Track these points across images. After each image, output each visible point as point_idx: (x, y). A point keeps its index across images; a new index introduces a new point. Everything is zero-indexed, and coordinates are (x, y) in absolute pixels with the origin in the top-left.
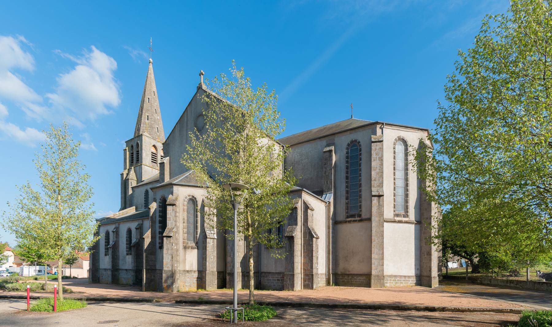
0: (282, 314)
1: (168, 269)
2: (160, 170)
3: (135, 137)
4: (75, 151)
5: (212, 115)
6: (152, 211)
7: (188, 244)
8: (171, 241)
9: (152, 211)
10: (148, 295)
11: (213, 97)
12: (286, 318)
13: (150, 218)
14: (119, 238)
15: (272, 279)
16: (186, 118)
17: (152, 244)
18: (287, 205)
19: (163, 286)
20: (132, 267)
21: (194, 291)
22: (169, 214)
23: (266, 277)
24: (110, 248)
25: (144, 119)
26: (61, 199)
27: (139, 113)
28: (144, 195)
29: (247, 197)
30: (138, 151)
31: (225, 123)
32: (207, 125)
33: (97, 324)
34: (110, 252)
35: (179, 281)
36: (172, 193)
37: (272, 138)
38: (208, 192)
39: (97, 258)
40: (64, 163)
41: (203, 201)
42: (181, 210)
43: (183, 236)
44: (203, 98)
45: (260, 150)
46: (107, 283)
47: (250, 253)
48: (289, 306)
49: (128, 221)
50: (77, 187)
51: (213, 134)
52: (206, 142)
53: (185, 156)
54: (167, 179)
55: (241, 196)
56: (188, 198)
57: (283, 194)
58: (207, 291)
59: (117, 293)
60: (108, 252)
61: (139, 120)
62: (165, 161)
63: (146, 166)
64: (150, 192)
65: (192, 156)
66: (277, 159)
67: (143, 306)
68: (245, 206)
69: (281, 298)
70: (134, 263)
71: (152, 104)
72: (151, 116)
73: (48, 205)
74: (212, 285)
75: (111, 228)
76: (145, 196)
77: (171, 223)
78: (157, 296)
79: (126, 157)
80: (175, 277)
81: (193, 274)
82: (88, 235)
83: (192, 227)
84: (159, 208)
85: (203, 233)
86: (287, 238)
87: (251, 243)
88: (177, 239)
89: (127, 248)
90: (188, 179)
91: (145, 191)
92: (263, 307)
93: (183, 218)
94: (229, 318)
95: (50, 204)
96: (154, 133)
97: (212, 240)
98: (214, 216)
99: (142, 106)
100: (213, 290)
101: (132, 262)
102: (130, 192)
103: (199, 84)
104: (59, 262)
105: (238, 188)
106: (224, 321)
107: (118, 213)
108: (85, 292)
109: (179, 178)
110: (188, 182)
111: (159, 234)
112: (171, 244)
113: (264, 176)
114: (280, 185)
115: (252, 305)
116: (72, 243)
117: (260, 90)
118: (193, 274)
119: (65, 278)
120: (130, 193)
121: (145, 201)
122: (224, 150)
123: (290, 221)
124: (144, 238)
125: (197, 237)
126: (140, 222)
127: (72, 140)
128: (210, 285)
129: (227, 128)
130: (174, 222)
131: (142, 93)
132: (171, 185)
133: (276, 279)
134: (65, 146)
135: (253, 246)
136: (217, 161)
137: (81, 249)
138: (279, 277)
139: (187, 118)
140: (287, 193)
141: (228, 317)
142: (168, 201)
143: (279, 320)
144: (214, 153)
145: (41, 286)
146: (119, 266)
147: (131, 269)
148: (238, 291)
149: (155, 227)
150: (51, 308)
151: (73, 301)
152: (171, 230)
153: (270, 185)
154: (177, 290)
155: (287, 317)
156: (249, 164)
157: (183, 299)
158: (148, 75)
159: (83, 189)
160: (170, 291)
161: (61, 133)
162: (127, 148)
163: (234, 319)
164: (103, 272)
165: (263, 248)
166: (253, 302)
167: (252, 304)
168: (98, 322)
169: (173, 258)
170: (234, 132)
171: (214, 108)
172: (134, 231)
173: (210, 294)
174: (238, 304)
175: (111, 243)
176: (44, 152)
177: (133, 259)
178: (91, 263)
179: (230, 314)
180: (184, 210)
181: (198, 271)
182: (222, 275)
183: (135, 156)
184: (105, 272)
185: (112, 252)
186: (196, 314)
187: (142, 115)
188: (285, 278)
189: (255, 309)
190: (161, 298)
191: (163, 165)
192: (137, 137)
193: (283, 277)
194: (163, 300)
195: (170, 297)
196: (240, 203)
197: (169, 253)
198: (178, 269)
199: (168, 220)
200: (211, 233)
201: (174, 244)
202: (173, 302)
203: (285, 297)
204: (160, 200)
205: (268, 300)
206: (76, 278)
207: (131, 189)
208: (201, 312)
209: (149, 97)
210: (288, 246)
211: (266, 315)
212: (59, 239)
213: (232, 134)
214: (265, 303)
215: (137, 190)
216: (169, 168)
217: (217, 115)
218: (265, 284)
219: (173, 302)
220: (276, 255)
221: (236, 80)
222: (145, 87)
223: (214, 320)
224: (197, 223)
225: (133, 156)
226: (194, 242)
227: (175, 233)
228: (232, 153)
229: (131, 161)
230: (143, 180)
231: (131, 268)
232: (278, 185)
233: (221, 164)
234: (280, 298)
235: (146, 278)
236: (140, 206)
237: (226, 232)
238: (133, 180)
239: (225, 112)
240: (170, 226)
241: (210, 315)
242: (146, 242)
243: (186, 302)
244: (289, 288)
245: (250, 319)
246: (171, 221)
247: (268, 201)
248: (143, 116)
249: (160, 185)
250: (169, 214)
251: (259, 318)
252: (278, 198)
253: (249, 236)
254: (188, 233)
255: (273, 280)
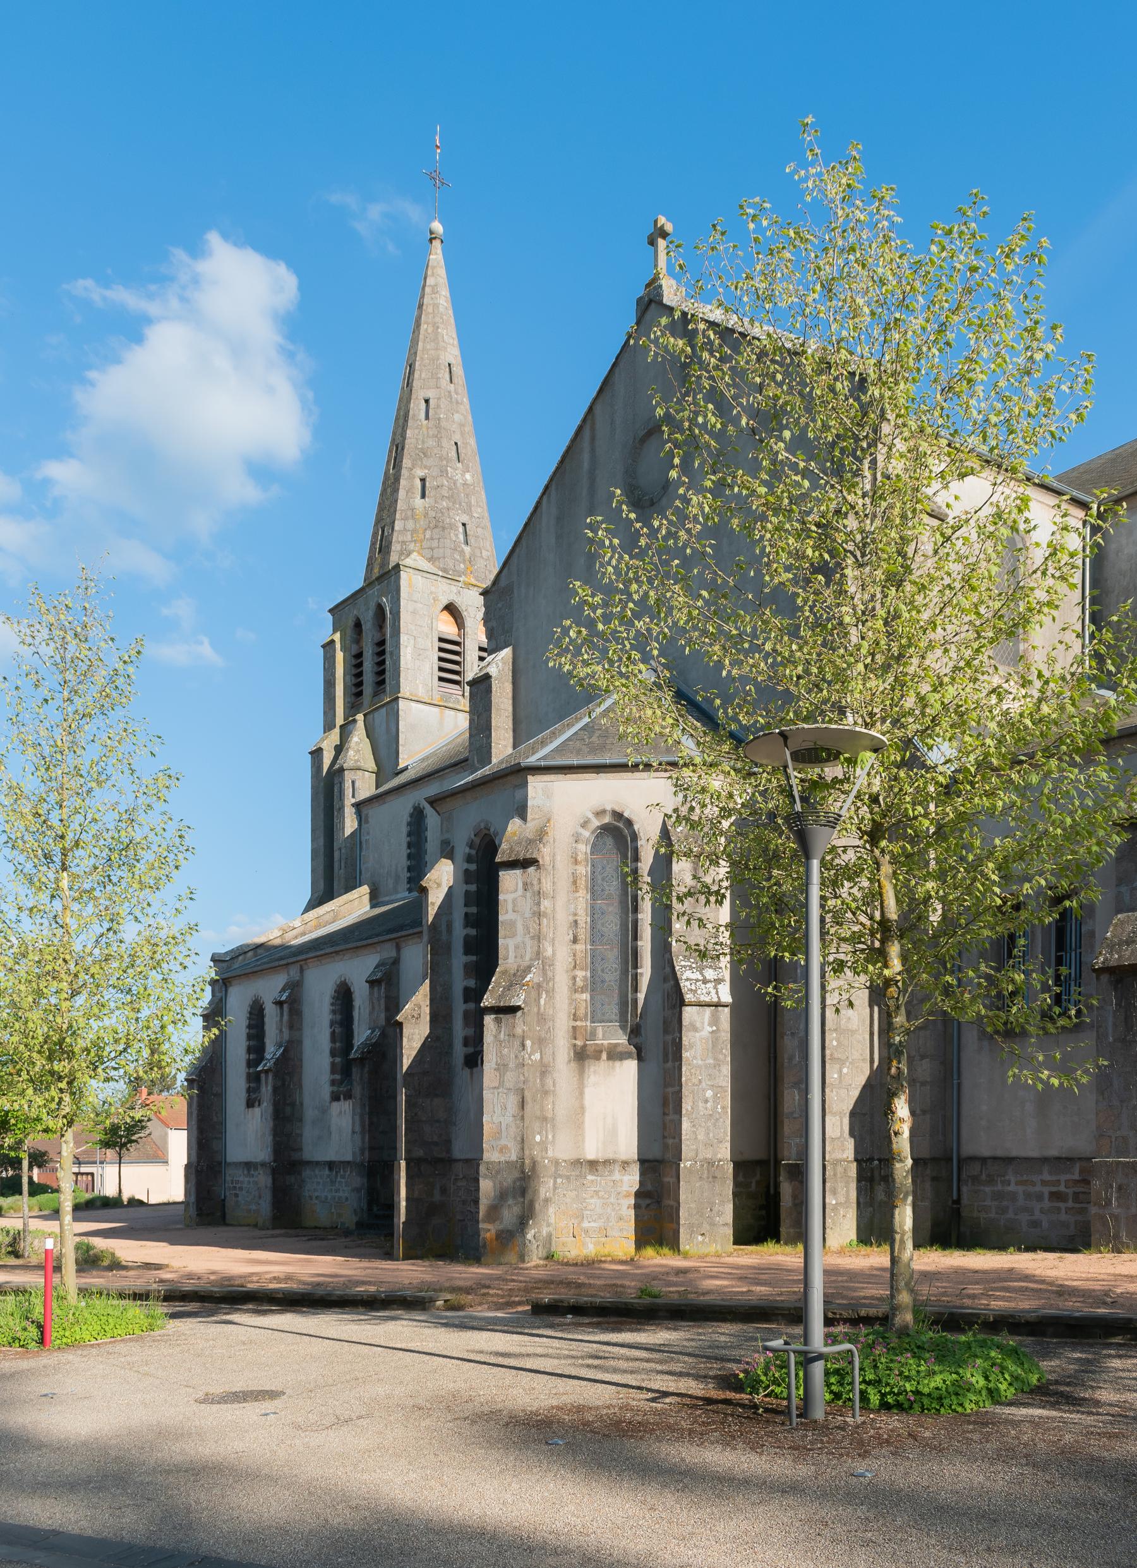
0: (1074, 1380)
1: (502, 1159)
2: (471, 712)
3: (369, 584)
4: (120, 681)
5: (696, 414)
6: (436, 899)
7: (593, 1035)
8: (519, 1031)
9: (436, 899)
10: (416, 1274)
11: (702, 326)
12: (1097, 1403)
13: (425, 929)
14: (300, 1029)
15: (1020, 1189)
16: (586, 457)
17: (434, 1046)
18: (1099, 806)
19: (482, 1233)
20: (354, 1154)
21: (621, 1255)
22: (510, 907)
23: (991, 1181)
24: (267, 1072)
25: (408, 498)
26: (71, 889)
27: (387, 470)
28: (404, 830)
29: (875, 789)
30: (382, 643)
31: (761, 441)
32: (673, 467)
33: (195, 1407)
34: (267, 1090)
35: (551, 1210)
36: (521, 811)
37: (1014, 471)
38: (680, 787)
39: (215, 1119)
40: (82, 738)
41: (665, 833)
42: (564, 883)
43: (572, 1001)
44: (656, 341)
45: (948, 539)
46: (256, 1226)
47: (893, 1071)
48: (1114, 1335)
49: (337, 952)
50: (129, 829)
51: (700, 504)
52: (667, 550)
53: (565, 632)
54: (502, 747)
55: (846, 786)
56: (596, 823)
57: (1077, 750)
58: (686, 1256)
59: (289, 1269)
60: (257, 1089)
61: (387, 503)
62: (493, 671)
63: (413, 704)
64: (432, 819)
65: (600, 627)
66: (1044, 573)
67: (391, 1326)
68: (864, 833)
69: (1072, 1292)
70: (363, 1133)
71: (443, 424)
72: (435, 478)
73: (24, 916)
74: (706, 1227)
75: (270, 988)
76: (409, 835)
77: (517, 947)
78: (451, 1279)
79: (333, 675)
80: (536, 1192)
81: (617, 1176)
82: (170, 1028)
83: (612, 956)
84: (467, 883)
85: (665, 980)
86: (1105, 978)
87: (900, 1019)
88: (542, 1018)
89: (333, 1072)
90: (594, 739)
91: (411, 815)
92: (963, 1338)
93: (571, 918)
94: (785, 1395)
95: (31, 910)
96: (448, 552)
97: (708, 1011)
98: (708, 902)
99: (398, 439)
100: (712, 1249)
101: (354, 1132)
102: (350, 824)
103: (648, 286)
104: (64, 1146)
105: (823, 749)
106: (755, 1407)
107: (297, 923)
108: (167, 1266)
109: (554, 735)
110: (593, 750)
111: (466, 1002)
112: (517, 1043)
113: (967, 669)
114: (1062, 708)
115: (903, 1332)
116: (113, 1064)
117: (950, 232)
118: (617, 1176)
119: (90, 1207)
120: (348, 831)
121: (409, 857)
122: (758, 572)
123: (1124, 889)
124: (400, 1025)
125: (635, 1001)
126: (389, 952)
127: (112, 639)
128: (700, 1225)
129: (774, 462)
130: (529, 942)
131: (399, 383)
132: (517, 774)
133: (1046, 1190)
134: (85, 668)
135: (908, 1032)
136: (720, 630)
137: (165, 1084)
138: (1064, 1180)
139: (593, 450)
140: (1102, 742)
141: (778, 1390)
142: (504, 846)
143: (1054, 1413)
144: (705, 593)
145: (8, 1240)
146: (301, 1149)
147: (349, 1162)
148: (841, 1252)
149: (449, 971)
150: (33, 1332)
151: (115, 1302)
152: (516, 979)
153: (1006, 713)
154: (542, 1252)
155: (1106, 1395)
156: (886, 624)
157: (568, 1296)
158: (423, 297)
159: (151, 835)
160: (512, 1257)
161: (70, 619)
162: (337, 637)
163: (807, 1399)
164: (240, 1176)
165: (970, 1038)
166: (909, 1317)
167: (906, 1327)
168: (200, 1395)
169: (528, 1107)
170: (806, 473)
171: (711, 378)
172: (361, 993)
173: (696, 1270)
174: (828, 1322)
175: (272, 1050)
176: (10, 704)
177: (357, 1118)
178: (194, 1141)
179: (788, 1374)
180: (575, 882)
181: (642, 1161)
182: (758, 1177)
183: (368, 666)
184: (249, 1175)
185: (275, 1090)
186: (625, 1371)
187: (397, 479)
188: (1096, 1184)
189: (918, 1351)
190: (468, 1291)
191: (482, 687)
192: (377, 579)
193: (1086, 1182)
194: (478, 1299)
195: (511, 1285)
196: (834, 822)
197: (508, 1085)
198: (550, 1153)
199: (502, 932)
200: (705, 981)
201: (528, 1043)
202: (520, 1309)
203: (1097, 1286)
204: (471, 846)
205: (999, 1304)
206: (140, 1203)
207: (354, 810)
208: (648, 1361)
209: (430, 394)
210: (1111, 1020)
211: (982, 1382)
212: (63, 1052)
213: (798, 485)
214: (977, 1316)
215: (375, 813)
216: (510, 695)
217: (722, 409)
218: (983, 1215)
219: (520, 1309)
220: (1036, 1070)
221: (822, 211)
222: (413, 352)
223: (709, 1401)
224: (635, 938)
225: (360, 665)
226: (623, 1028)
227: (534, 994)
228: (795, 581)
229: (354, 690)
230: (401, 766)
231: (349, 1157)
232: (1045, 709)
233: (743, 641)
234: (1063, 1291)
235: (408, 1199)
236: (391, 882)
237: (775, 971)
238: (360, 773)
239: (760, 388)
240: (511, 960)
241: (688, 1375)
242: (409, 1040)
243: (578, 1310)
244: (1117, 1237)
245: (890, 1399)
246: (519, 939)
247: (990, 794)
248: (403, 482)
249: (470, 778)
250: (510, 907)
251: (940, 1398)
252: (1050, 772)
253: (888, 982)
254: (595, 985)
255: (1028, 1196)
